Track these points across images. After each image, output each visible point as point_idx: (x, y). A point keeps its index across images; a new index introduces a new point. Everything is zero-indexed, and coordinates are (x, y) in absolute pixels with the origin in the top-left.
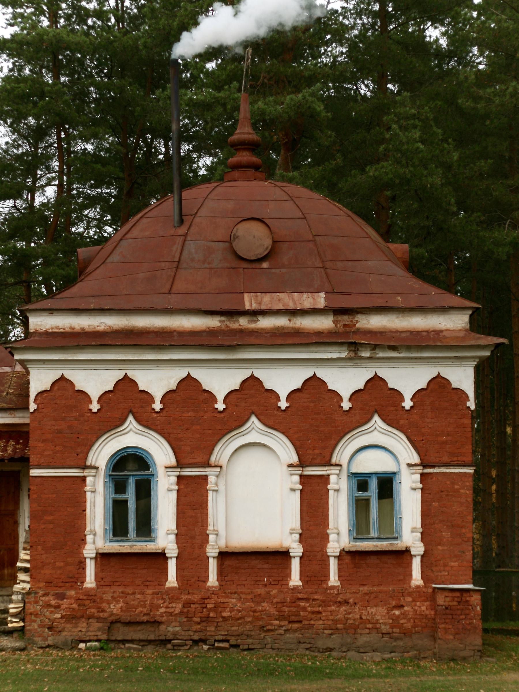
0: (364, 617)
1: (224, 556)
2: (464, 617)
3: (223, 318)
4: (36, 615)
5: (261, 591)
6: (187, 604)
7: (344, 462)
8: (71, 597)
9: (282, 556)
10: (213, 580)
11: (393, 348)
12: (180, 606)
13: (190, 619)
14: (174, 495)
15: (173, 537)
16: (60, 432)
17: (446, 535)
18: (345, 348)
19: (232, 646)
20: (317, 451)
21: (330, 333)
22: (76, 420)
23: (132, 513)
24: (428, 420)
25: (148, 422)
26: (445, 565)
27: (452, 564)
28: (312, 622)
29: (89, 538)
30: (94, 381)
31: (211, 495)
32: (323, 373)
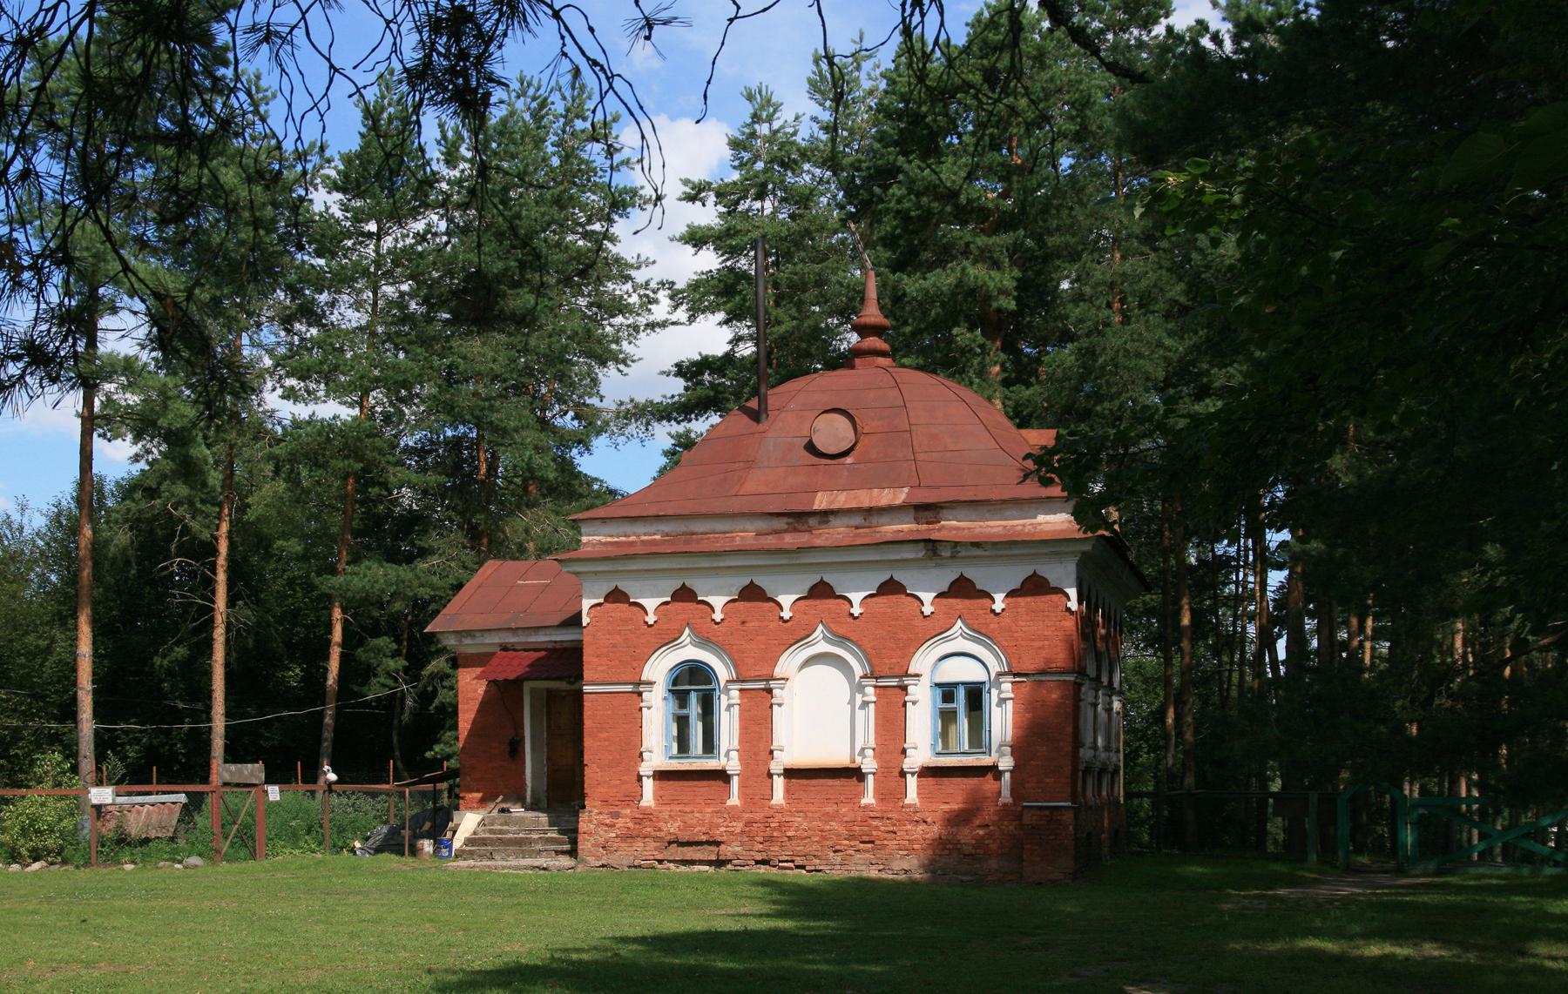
1: (790, 773)
4: (590, 834)
5: (831, 809)
6: (749, 823)
8: (626, 816)
10: (912, 795)
13: (752, 838)
16: (614, 646)
19: (798, 867)
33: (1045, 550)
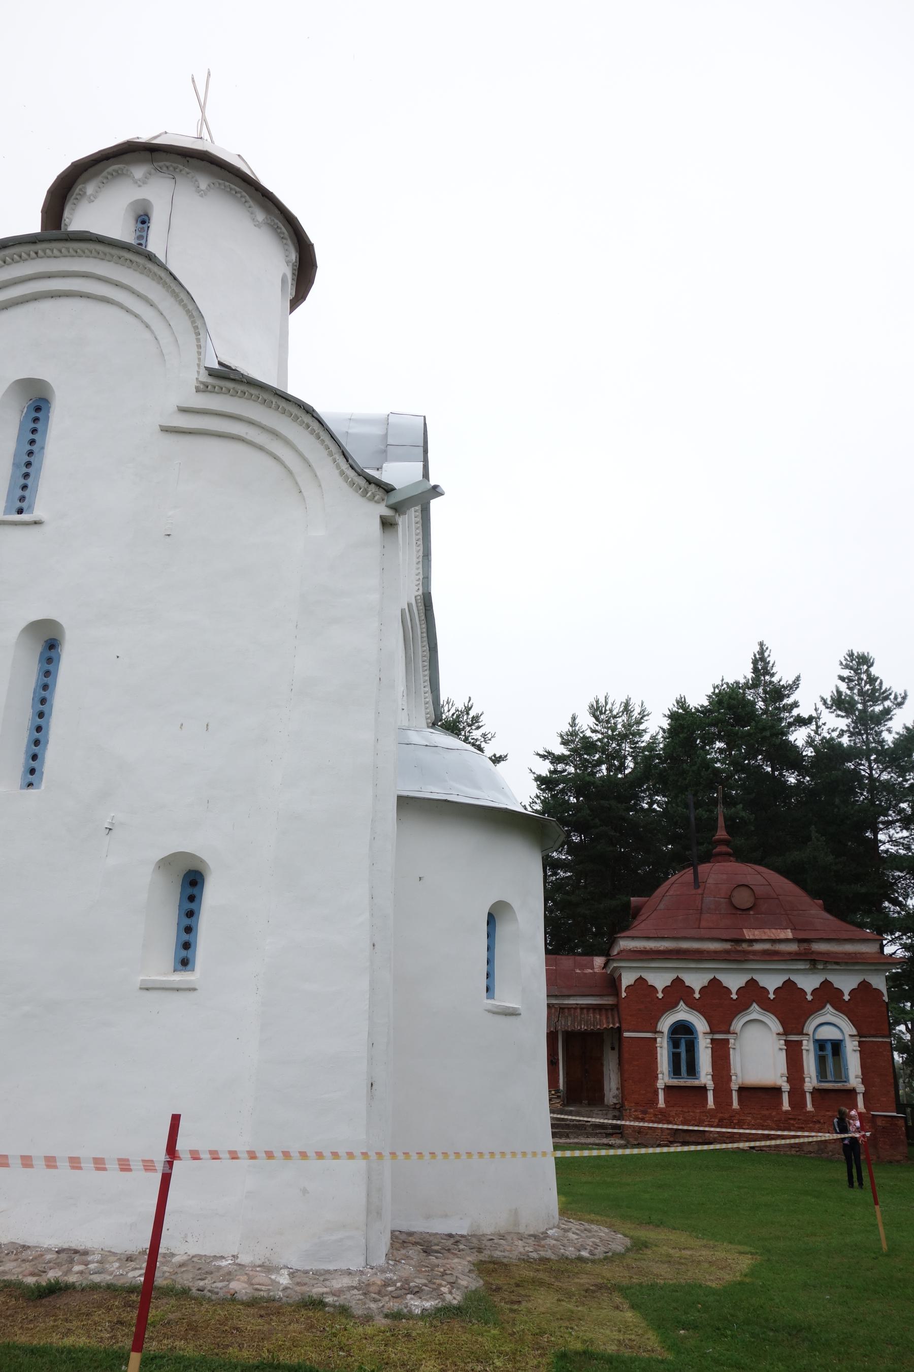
1: (742, 1090)
7: (811, 1032)
9: (776, 1091)
10: (735, 1105)
11: (837, 963)
12: (717, 1120)
14: (709, 1051)
15: (710, 1077)
18: (808, 962)
21: (796, 954)
22: (649, 1004)
23: (683, 1060)
25: (693, 1005)
29: (660, 1076)
30: (660, 980)
31: (731, 1051)
32: (794, 978)
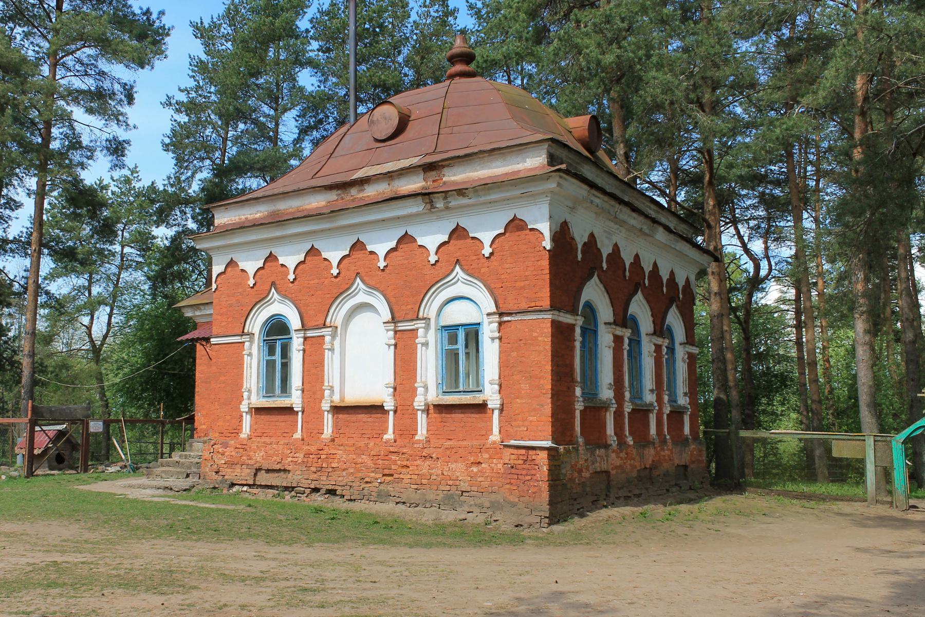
0: (445, 473)
1: (337, 410)
2: (529, 477)
3: (339, 192)
6: (307, 455)
9: (377, 409)
17: (525, 386)
20: (409, 307)
24: (507, 266)
25: (285, 295)
26: (524, 420)
27: (531, 418)
28: (401, 476)
31: (327, 354)
33: (517, 192)
